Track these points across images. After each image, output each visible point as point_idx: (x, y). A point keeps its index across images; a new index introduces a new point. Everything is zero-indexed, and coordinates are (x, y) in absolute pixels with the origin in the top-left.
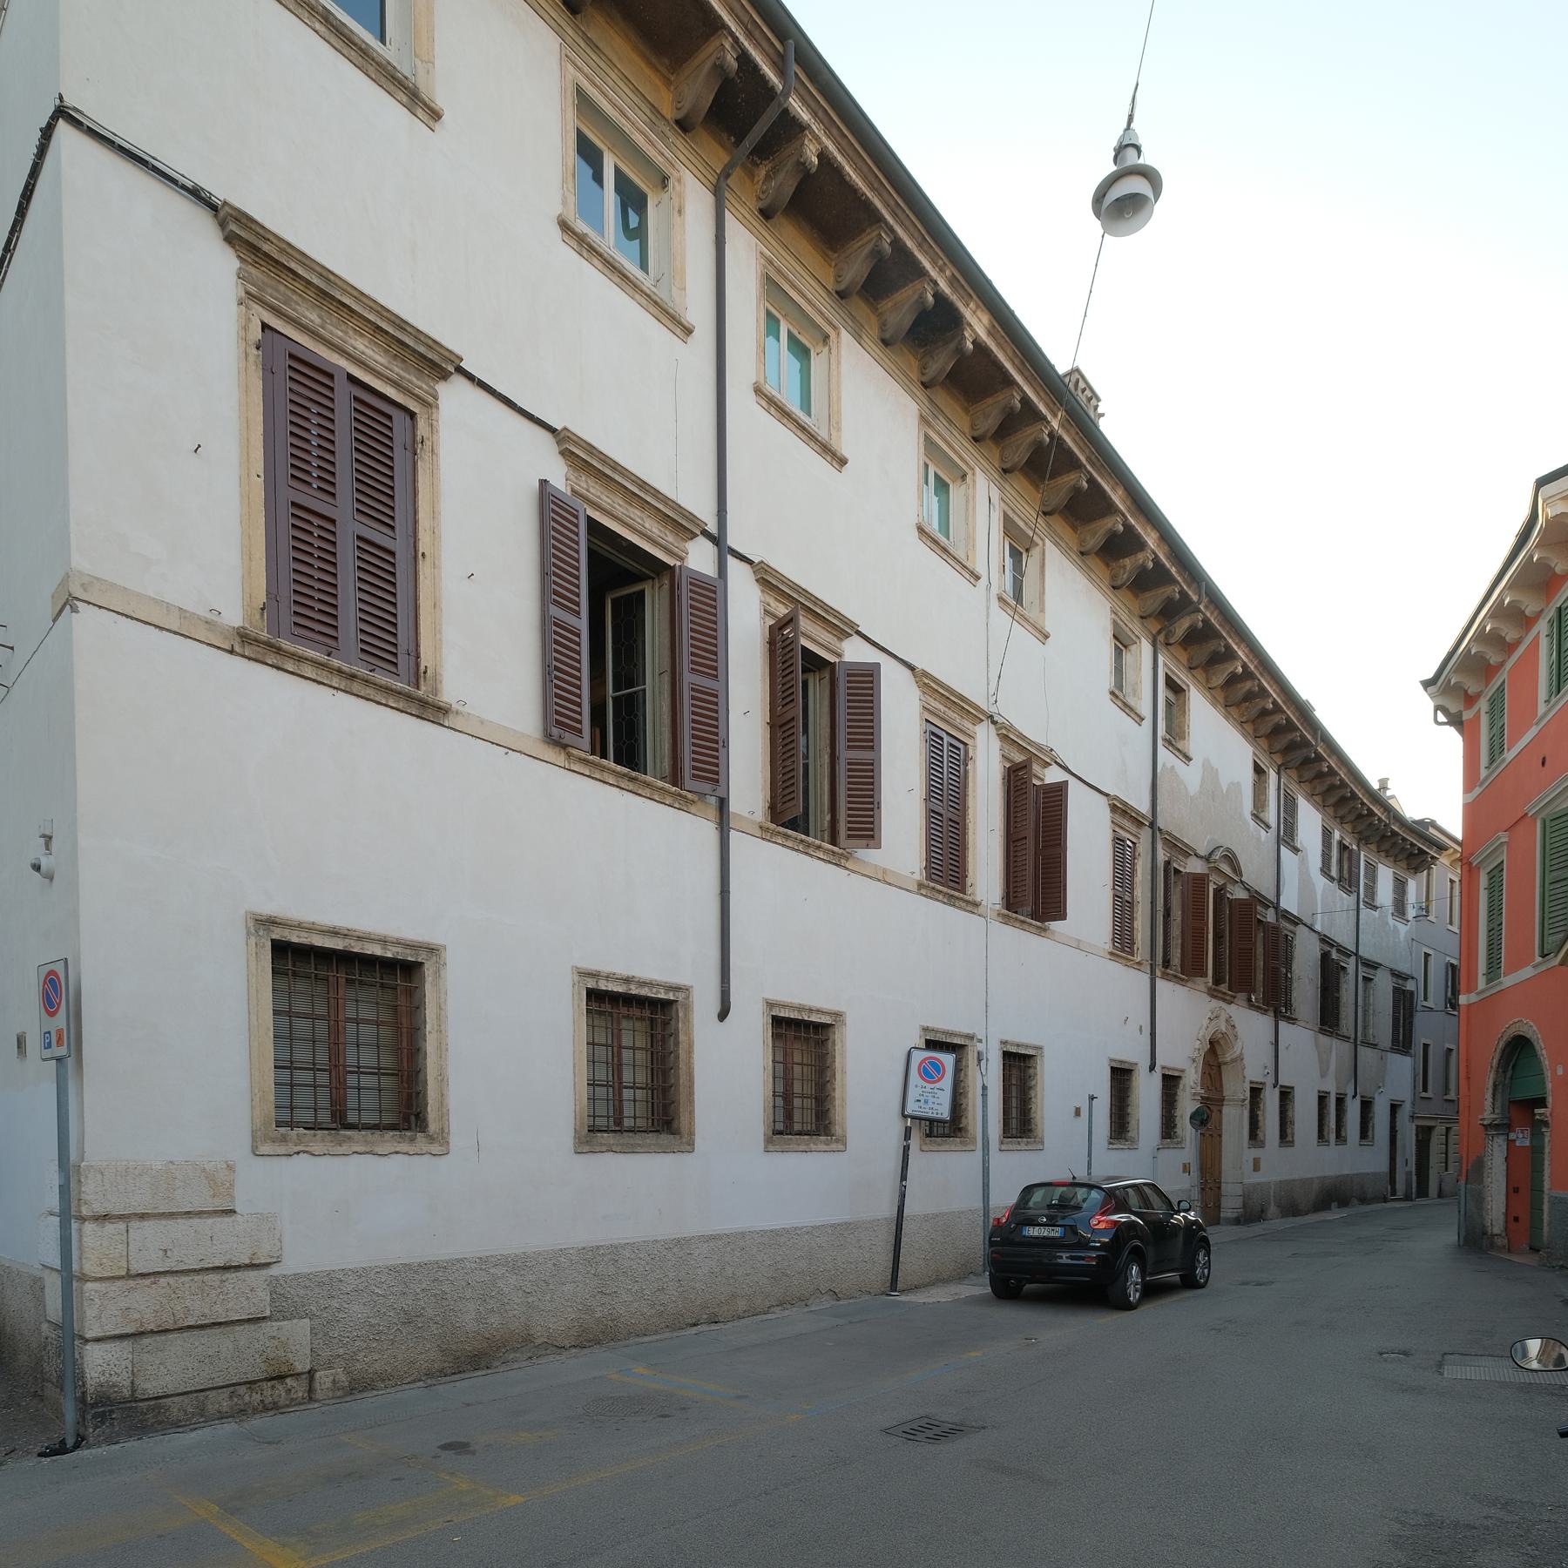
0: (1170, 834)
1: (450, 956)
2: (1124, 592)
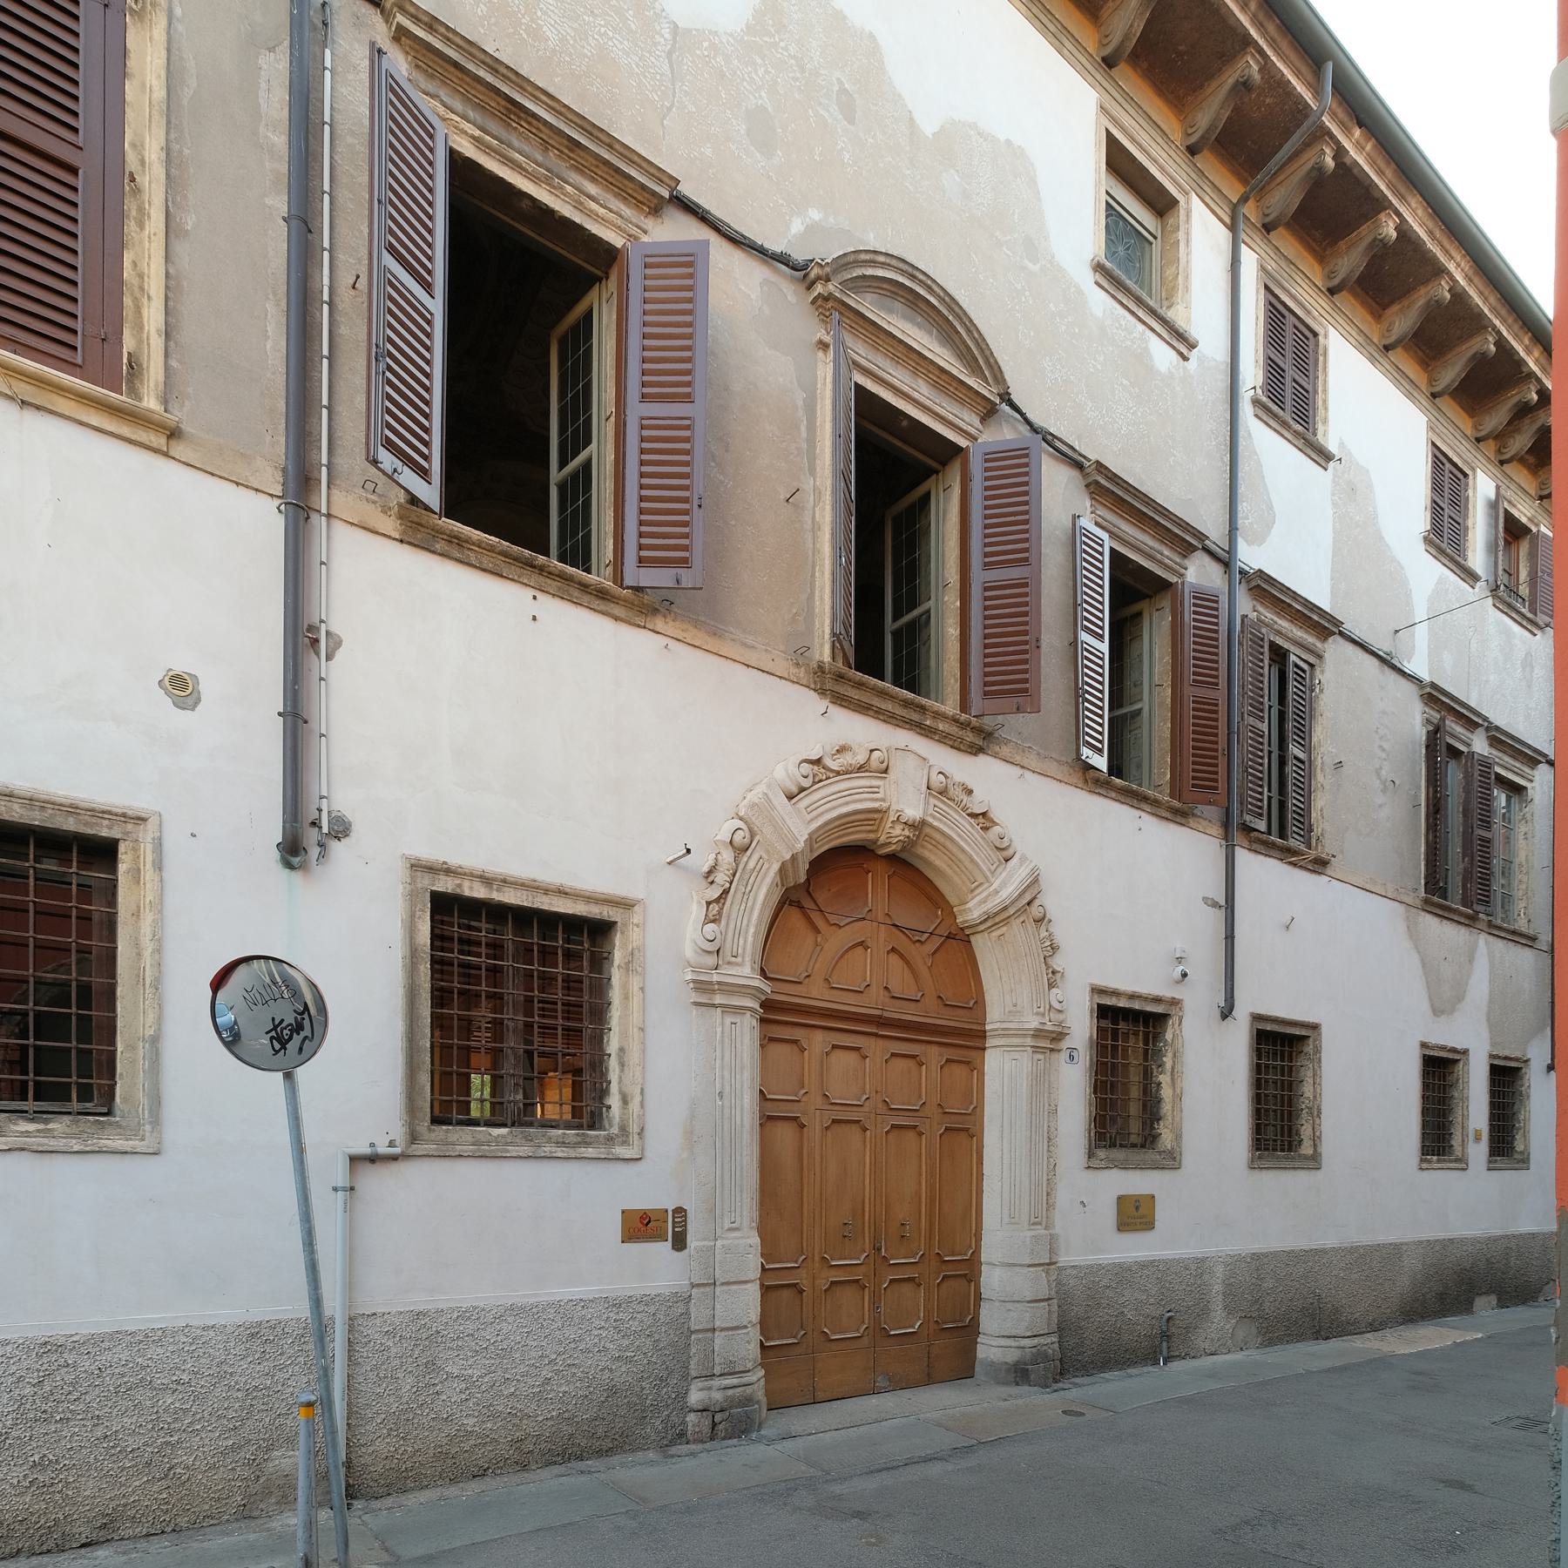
0: (1100, 466)
1: (1324, 1030)
2: (1446, 404)
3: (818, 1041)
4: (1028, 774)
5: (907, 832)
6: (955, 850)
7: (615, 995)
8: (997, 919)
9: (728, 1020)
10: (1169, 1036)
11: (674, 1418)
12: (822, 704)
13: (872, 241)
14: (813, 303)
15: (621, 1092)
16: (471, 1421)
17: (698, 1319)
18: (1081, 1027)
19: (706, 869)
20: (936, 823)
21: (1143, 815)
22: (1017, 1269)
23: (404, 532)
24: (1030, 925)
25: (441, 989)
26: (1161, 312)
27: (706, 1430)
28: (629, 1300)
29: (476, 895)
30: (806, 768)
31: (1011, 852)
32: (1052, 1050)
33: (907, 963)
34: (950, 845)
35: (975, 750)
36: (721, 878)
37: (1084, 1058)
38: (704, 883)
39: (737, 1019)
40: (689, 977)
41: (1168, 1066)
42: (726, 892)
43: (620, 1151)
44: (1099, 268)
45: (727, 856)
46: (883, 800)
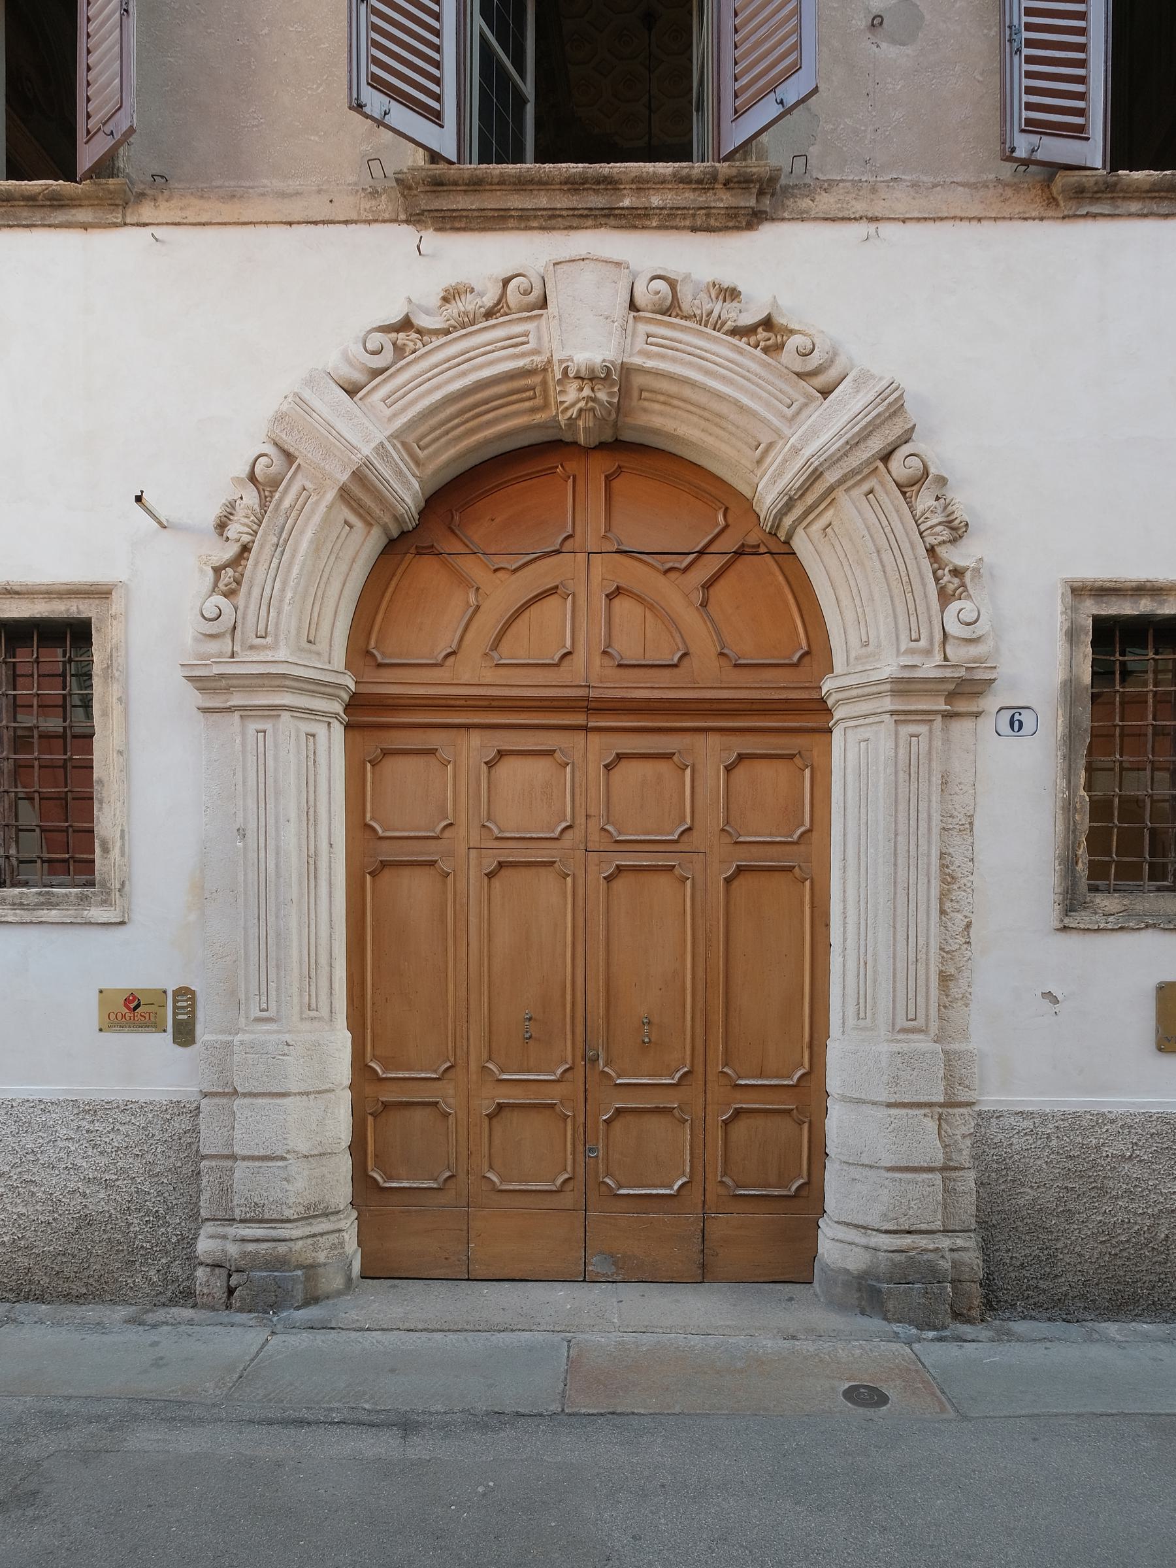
3: (474, 748)
6: (702, 398)
8: (810, 499)
9: (253, 726)
11: (176, 1269)
12: (406, 234)
17: (210, 1140)
20: (650, 364)
22: (867, 1110)
24: (891, 498)
27: (219, 1292)
28: (109, 1106)
32: (948, 716)
34: (687, 392)
35: (753, 219)
37: (1049, 724)
39: (268, 726)
42: (245, 549)
45: (251, 497)
46: (536, 352)
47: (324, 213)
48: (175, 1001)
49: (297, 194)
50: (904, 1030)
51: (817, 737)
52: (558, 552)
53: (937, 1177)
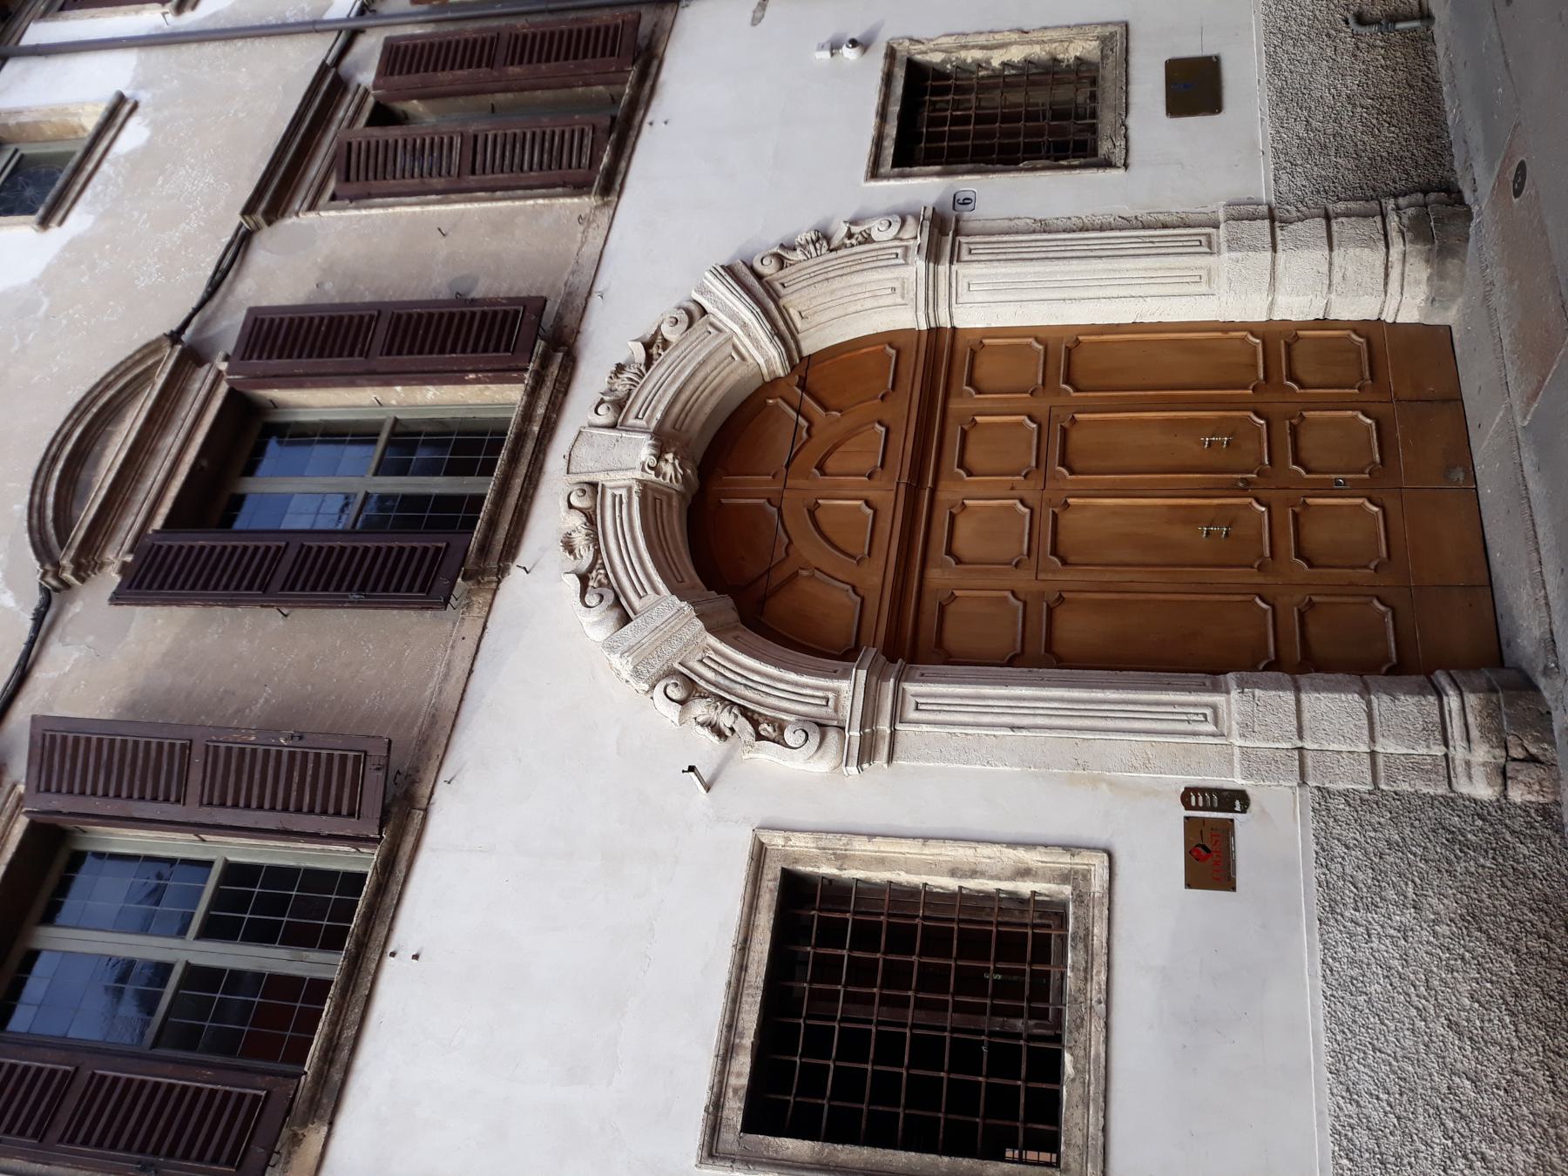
0: (248, 210)
4: (599, 287)
5: (670, 457)
7: (879, 876)
10: (936, 58)
12: (515, 575)
13: (20, 508)
14: (83, 580)
15: (1012, 878)
16: (1519, 1157)
18: (926, 188)
19: (715, 739)
20: (658, 415)
21: (648, 119)
22: (1280, 268)
23: (321, 1119)
25: (1074, 150)
26: (86, 143)
27: (1537, 772)
29: (747, 1069)
30: (592, 599)
31: (693, 307)
33: (836, 447)
34: (684, 397)
36: (726, 719)
37: (967, 183)
38: (733, 739)
39: (910, 703)
40: (853, 769)
41: (978, 54)
42: (745, 712)
43: (1098, 885)
44: (44, 223)
45: (700, 709)
46: (629, 489)
47: (470, 644)
48: (1197, 808)
49: (448, 665)
50: (1210, 247)
51: (959, 336)
52: (780, 509)
53: (1333, 222)
